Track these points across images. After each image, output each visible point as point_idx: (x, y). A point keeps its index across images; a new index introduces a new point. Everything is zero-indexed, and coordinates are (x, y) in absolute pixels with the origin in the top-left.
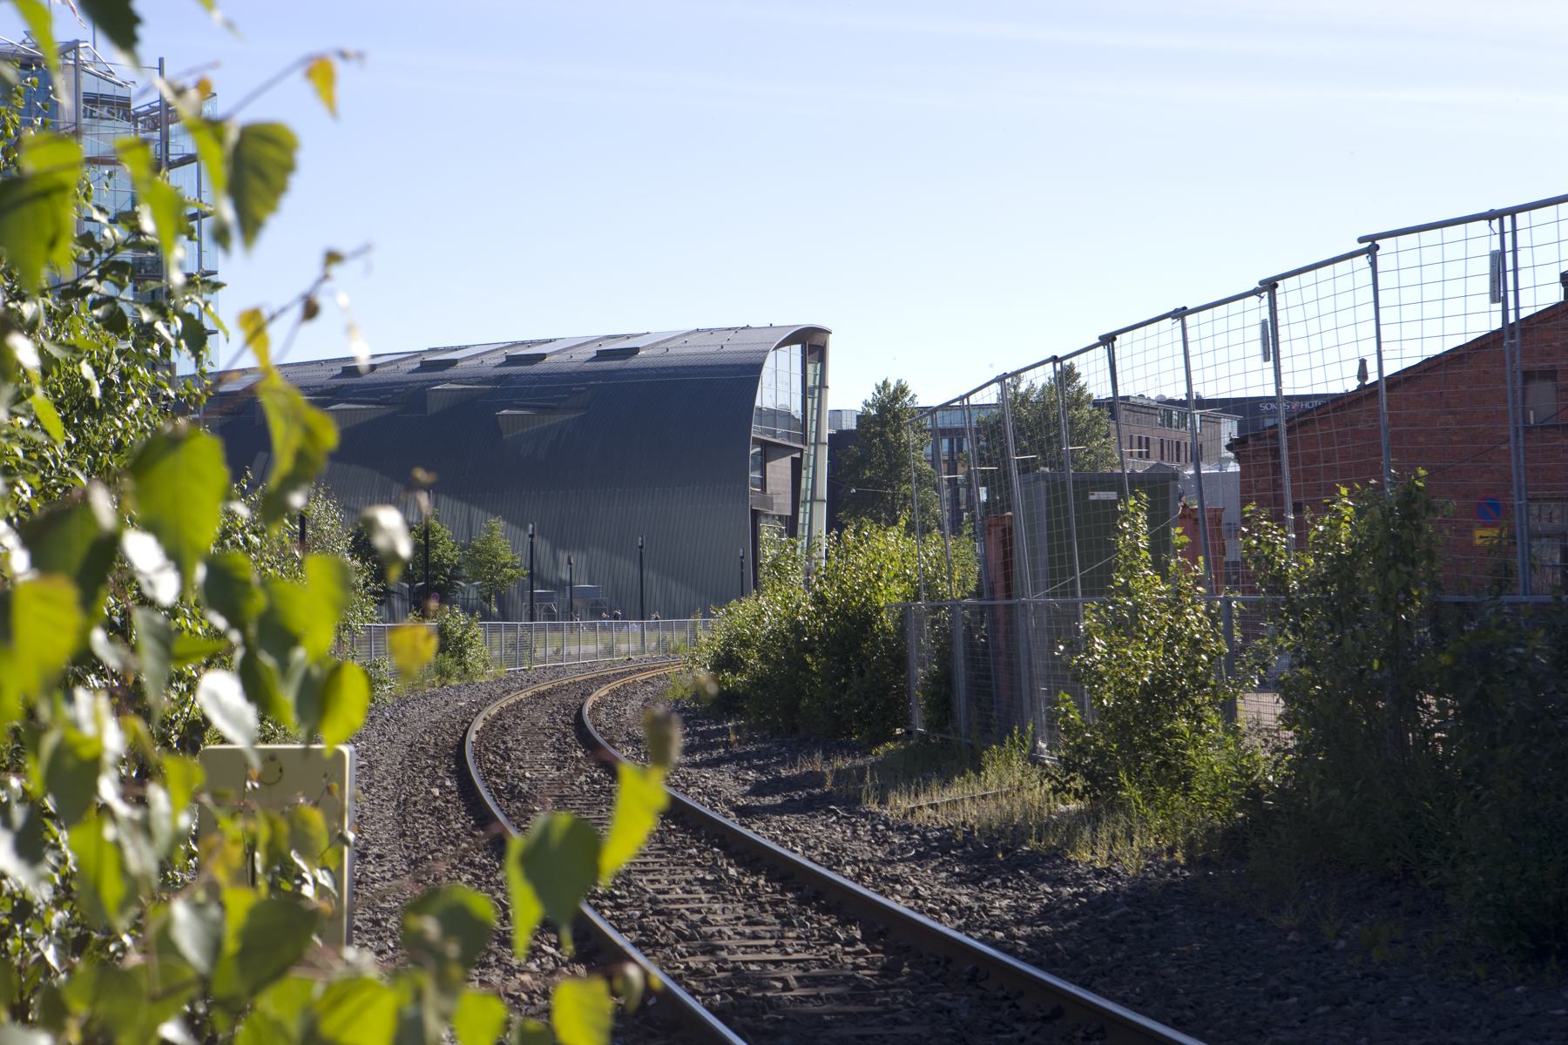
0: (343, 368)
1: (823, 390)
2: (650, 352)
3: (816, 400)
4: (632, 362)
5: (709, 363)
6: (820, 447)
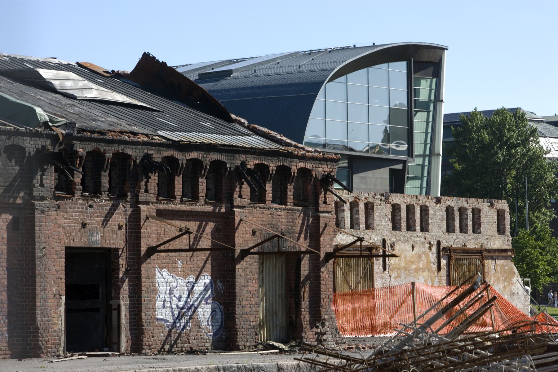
0: (199, 74)
1: (438, 103)
2: (243, 74)
3: (431, 113)
4: (224, 84)
5: (277, 83)
6: (434, 159)
